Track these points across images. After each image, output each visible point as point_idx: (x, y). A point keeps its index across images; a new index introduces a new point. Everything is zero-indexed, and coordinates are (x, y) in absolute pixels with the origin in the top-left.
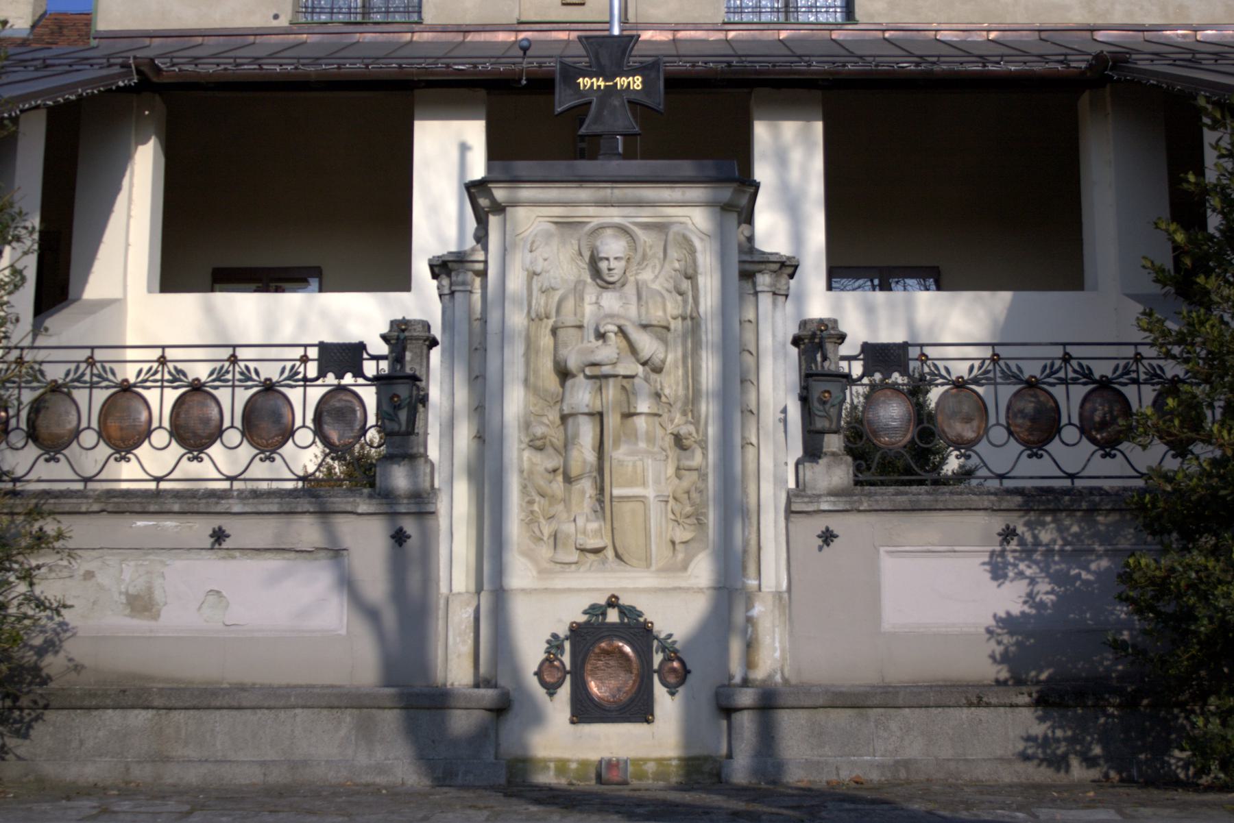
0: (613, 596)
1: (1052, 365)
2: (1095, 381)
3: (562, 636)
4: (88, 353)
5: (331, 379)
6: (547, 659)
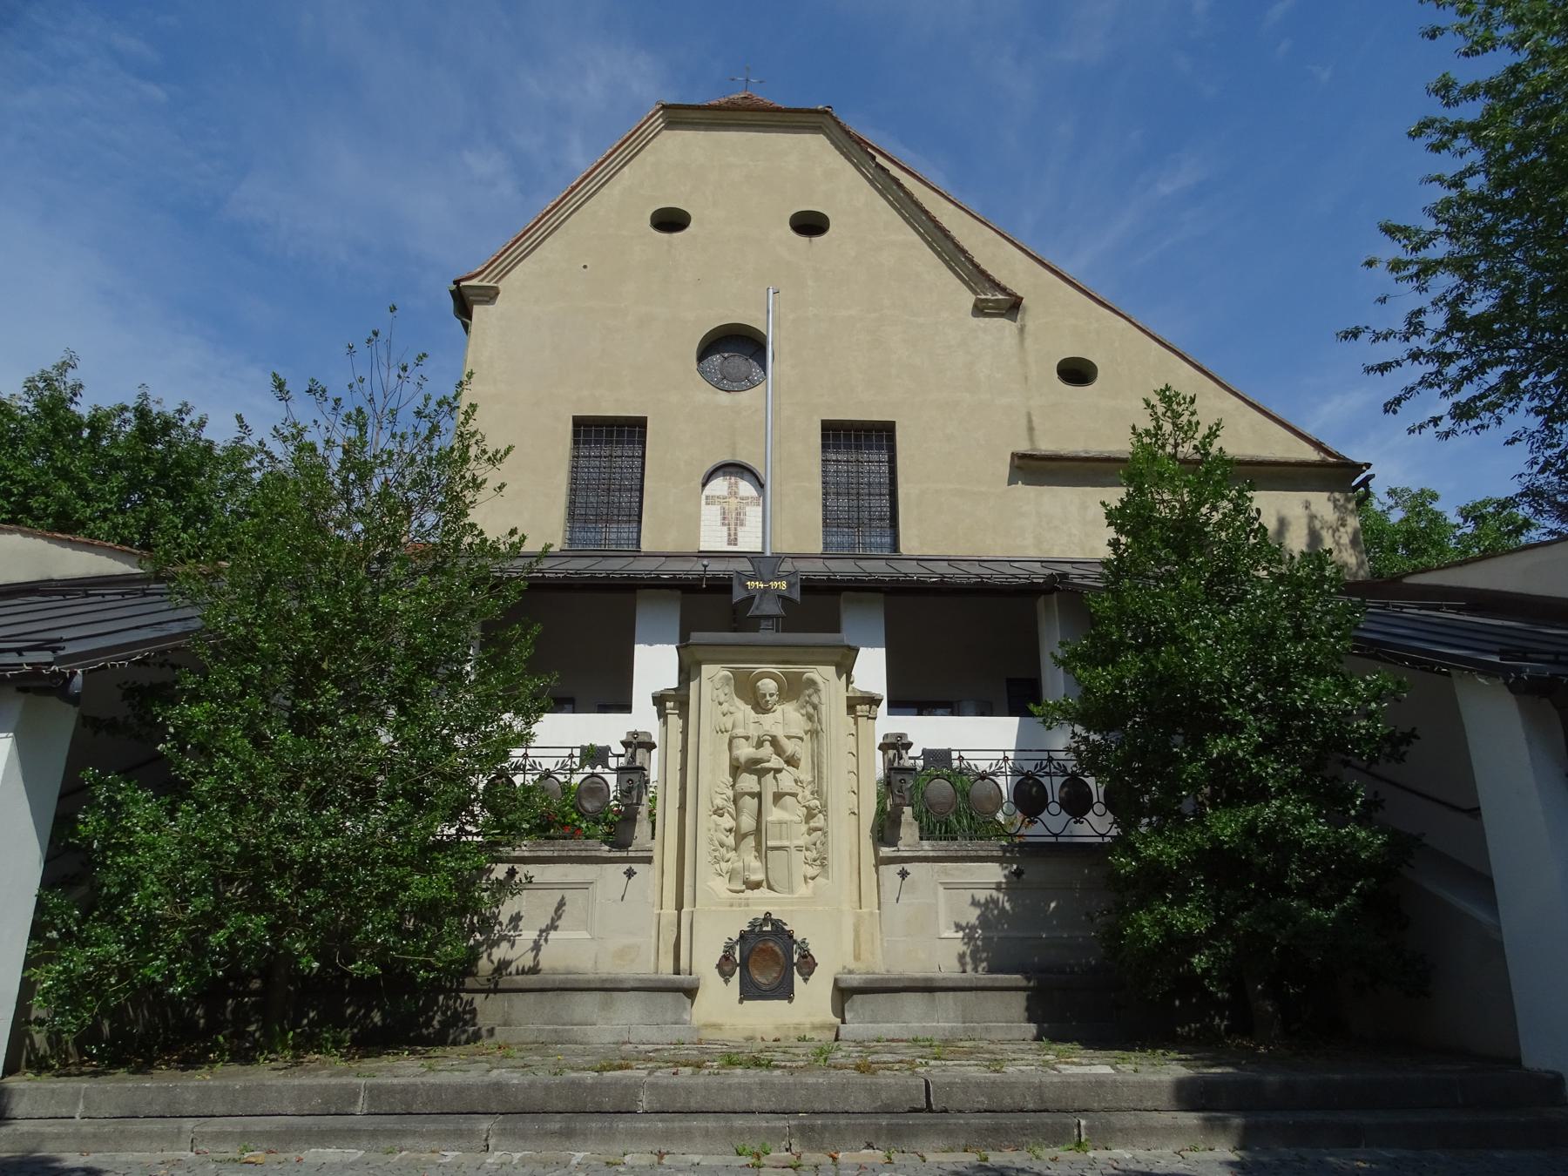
5: (588, 769)
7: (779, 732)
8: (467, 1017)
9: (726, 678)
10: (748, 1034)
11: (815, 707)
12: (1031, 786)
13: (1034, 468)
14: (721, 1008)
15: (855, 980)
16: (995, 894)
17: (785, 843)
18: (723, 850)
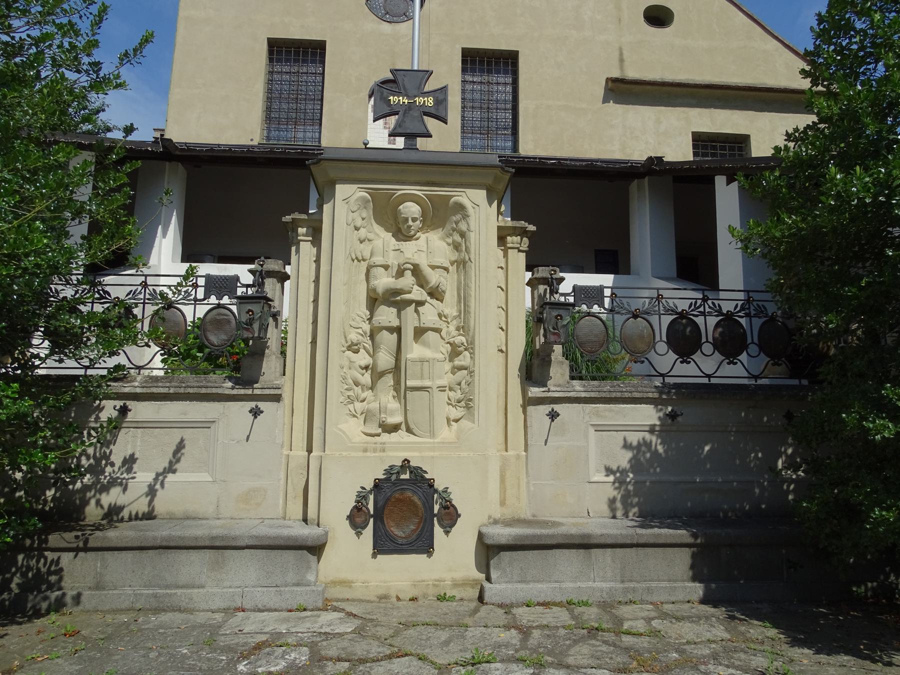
0: (406, 460)
1: (696, 303)
2: (722, 314)
3: (368, 489)
4: (143, 278)
5: (213, 299)
6: (355, 507)
7: (423, 261)
8: (53, 578)
9: (363, 198)
10: (381, 592)
11: (463, 235)
12: (685, 326)
13: (622, 90)
14: (351, 560)
15: (502, 534)
16: (648, 436)
17: (427, 383)
18: (358, 390)
